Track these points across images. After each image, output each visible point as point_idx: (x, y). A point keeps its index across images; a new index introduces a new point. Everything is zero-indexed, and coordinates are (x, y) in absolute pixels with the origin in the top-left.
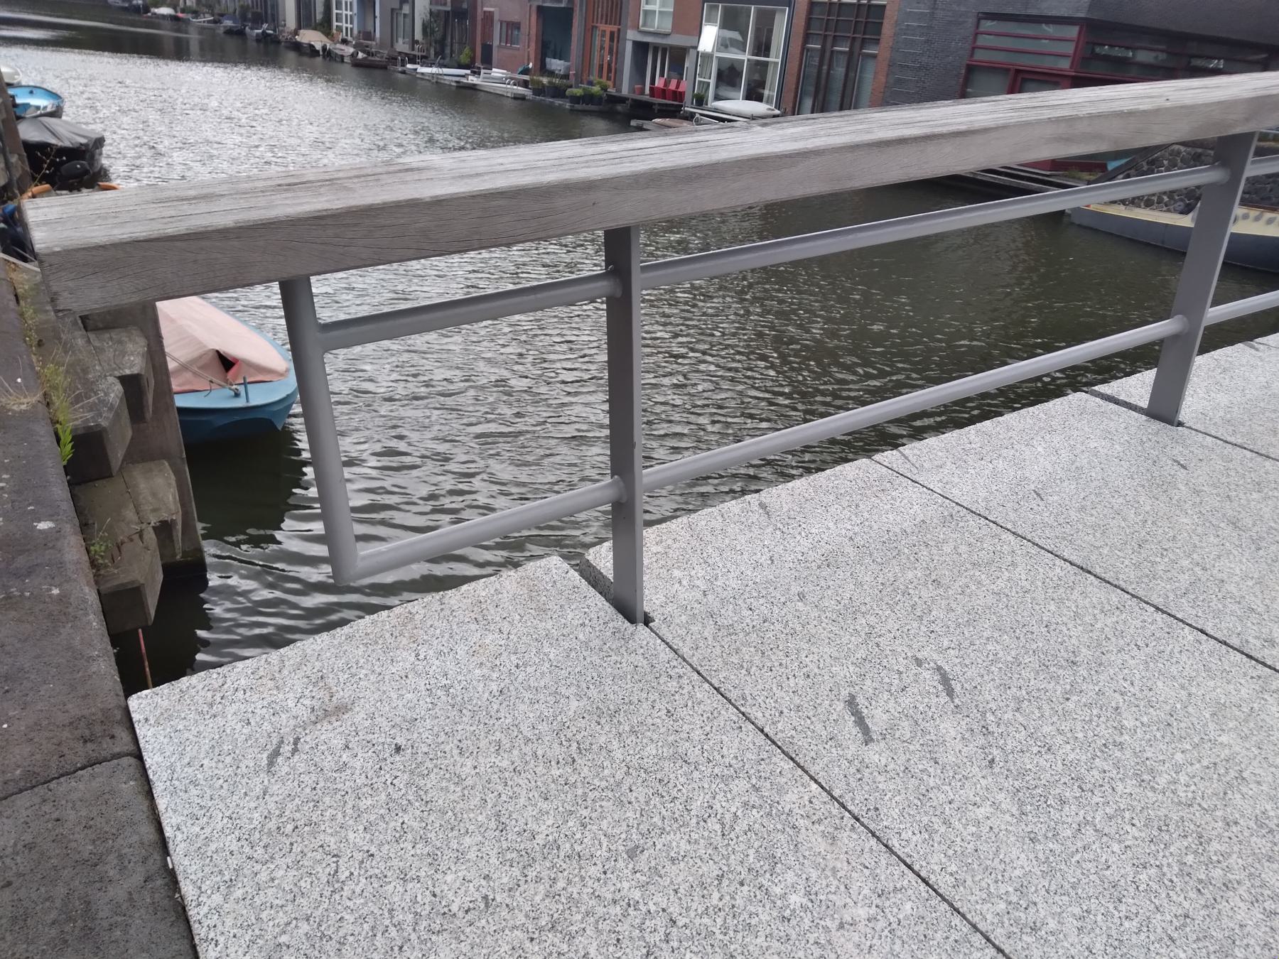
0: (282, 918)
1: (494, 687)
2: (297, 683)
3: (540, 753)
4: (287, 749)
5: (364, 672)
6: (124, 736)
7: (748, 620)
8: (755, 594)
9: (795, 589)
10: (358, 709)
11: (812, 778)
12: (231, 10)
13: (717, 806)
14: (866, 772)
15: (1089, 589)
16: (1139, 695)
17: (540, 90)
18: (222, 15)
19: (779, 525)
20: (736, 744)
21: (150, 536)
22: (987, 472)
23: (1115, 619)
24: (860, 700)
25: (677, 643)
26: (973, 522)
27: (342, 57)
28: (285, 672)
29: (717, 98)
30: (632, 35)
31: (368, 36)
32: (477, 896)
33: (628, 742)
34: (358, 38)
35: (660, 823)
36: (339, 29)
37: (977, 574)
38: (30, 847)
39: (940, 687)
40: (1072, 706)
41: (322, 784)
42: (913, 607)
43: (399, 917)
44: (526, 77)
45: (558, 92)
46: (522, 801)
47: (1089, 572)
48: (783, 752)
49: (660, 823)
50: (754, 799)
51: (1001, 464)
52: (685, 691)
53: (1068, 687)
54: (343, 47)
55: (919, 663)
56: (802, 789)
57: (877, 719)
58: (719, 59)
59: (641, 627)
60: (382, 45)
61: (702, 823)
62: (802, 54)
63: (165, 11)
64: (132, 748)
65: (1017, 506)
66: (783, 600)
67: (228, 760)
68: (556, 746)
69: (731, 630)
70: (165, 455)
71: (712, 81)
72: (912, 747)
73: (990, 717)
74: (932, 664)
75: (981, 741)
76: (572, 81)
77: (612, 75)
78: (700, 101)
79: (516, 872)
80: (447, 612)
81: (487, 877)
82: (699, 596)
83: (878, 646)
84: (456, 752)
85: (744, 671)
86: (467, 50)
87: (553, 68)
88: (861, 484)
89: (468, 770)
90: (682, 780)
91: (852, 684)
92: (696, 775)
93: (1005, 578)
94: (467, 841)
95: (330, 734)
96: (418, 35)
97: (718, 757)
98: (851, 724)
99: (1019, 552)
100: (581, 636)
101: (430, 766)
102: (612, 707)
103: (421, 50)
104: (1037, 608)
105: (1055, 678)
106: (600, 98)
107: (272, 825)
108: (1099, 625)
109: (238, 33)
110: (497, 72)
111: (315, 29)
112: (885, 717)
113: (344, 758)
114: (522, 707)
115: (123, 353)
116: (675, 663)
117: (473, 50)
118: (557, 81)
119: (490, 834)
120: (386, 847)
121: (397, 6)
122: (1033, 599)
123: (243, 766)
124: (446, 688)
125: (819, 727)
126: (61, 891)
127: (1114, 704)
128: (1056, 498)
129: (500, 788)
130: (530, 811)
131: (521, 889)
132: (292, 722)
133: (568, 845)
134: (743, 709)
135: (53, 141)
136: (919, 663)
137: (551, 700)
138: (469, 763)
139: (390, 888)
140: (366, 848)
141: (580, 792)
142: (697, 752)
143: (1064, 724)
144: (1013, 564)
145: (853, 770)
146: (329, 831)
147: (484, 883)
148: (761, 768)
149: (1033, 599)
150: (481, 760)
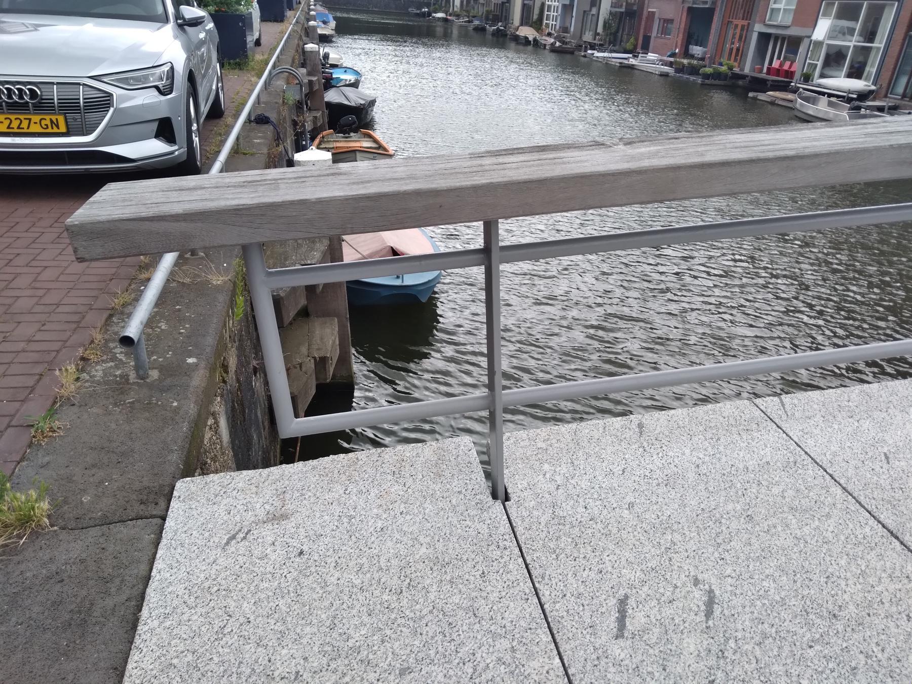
0: (181, 648)
1: (379, 524)
2: (268, 492)
3: (383, 580)
4: (241, 535)
5: (310, 494)
6: (162, 504)
7: (579, 516)
8: (596, 496)
9: (630, 498)
10: (292, 519)
11: (559, 654)
12: (480, 14)
13: (478, 656)
14: (603, 662)
15: (889, 553)
16: (884, 663)
17: (680, 69)
18: (474, 17)
19: (645, 444)
20: (517, 612)
21: (311, 365)
22: (850, 429)
23: (900, 586)
24: (632, 602)
25: (517, 522)
26: (812, 470)
27: (545, 45)
28: (266, 484)
29: (822, 76)
30: (758, 28)
31: (565, 30)
32: (294, 670)
33: (444, 588)
34: (559, 32)
35: (433, 655)
36: (547, 25)
37: (790, 517)
38: (82, 561)
39: (703, 608)
40: (812, 654)
41: (247, 565)
42: (718, 535)
43: (243, 668)
44: (672, 59)
45: (694, 70)
46: (354, 612)
47: (897, 538)
48: (549, 627)
49: (433, 655)
50: (508, 658)
51: (866, 424)
52: (503, 560)
53: (818, 636)
54: (547, 38)
55: (696, 582)
56: (547, 660)
57: (636, 620)
58: (828, 45)
59: (498, 503)
60: (573, 37)
61: (461, 665)
62: (904, 40)
63: (440, 15)
64: (163, 513)
65: (860, 464)
66: (614, 506)
67: (207, 535)
68: (396, 578)
69: (562, 521)
70: (337, 315)
71: (820, 64)
72: (651, 651)
73: (732, 643)
74: (707, 587)
75: (712, 661)
76: (707, 62)
77: (739, 58)
78: (807, 78)
79: (325, 661)
80: (379, 463)
81: (306, 659)
82: (552, 487)
83: (670, 559)
84: (333, 564)
85: (554, 556)
86: (632, 40)
87: (694, 52)
88: (732, 421)
89: (333, 580)
90: (465, 628)
91: (631, 587)
92: (477, 626)
93: (813, 526)
94: (308, 629)
95: (268, 533)
96: (600, 29)
97: (499, 618)
98: (613, 619)
99: (839, 506)
100: (454, 502)
101: (313, 570)
102: (446, 560)
103: (600, 40)
104: (829, 558)
105: (810, 625)
106: (726, 75)
107: (207, 584)
108: (879, 589)
109: (480, 30)
110: (651, 56)
111: (531, 26)
112: (643, 620)
113: (268, 551)
114: (389, 544)
115: (312, 249)
116: (507, 537)
117: (637, 40)
118: (695, 62)
119: (323, 629)
120: (260, 619)
121: (587, 8)
122: (829, 550)
123: (212, 541)
124: (351, 517)
125: (588, 614)
126: (84, 593)
127: (853, 664)
128: (903, 463)
129: (346, 598)
130: (356, 621)
131: (321, 674)
132: (253, 519)
133: (366, 653)
134: (537, 585)
135: (346, 103)
136: (696, 582)
137: (410, 543)
138: (337, 575)
139: (248, 647)
140: (248, 616)
141: (393, 616)
142: (487, 610)
143: (795, 667)
144: (828, 516)
145: (594, 656)
146: (235, 598)
147: (302, 662)
148: (525, 635)
149: (829, 550)
150: (345, 575)
